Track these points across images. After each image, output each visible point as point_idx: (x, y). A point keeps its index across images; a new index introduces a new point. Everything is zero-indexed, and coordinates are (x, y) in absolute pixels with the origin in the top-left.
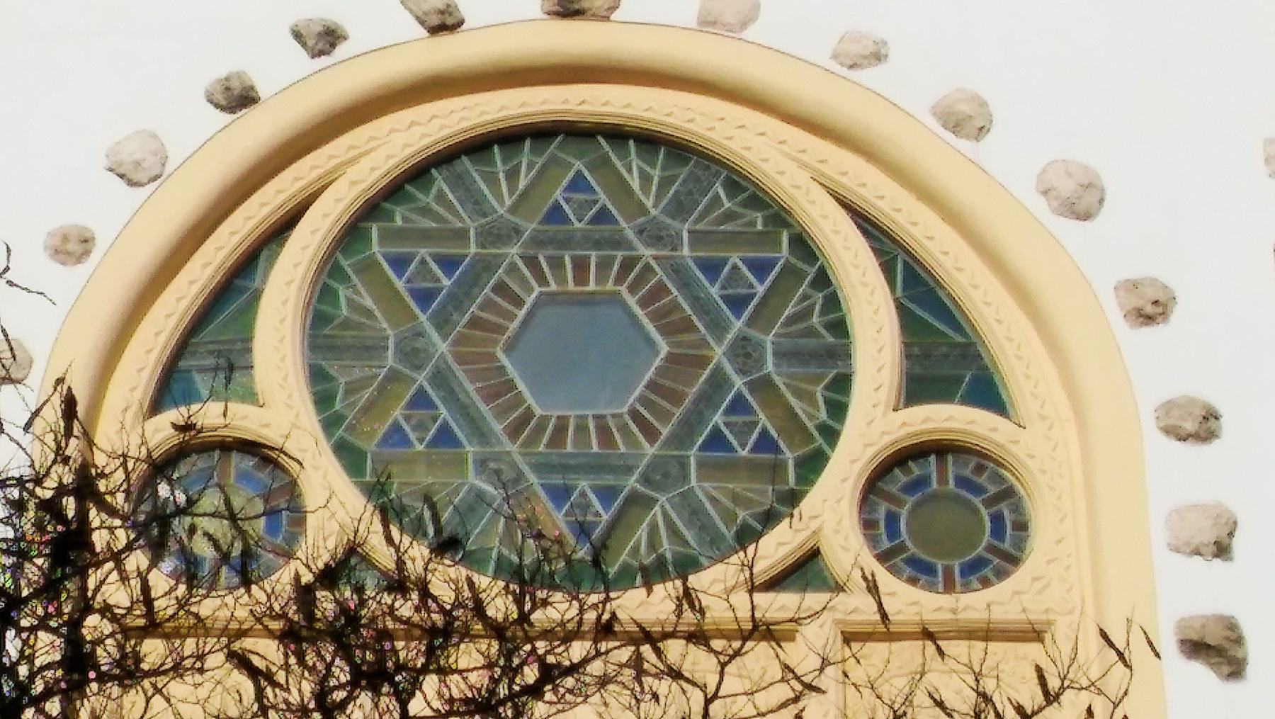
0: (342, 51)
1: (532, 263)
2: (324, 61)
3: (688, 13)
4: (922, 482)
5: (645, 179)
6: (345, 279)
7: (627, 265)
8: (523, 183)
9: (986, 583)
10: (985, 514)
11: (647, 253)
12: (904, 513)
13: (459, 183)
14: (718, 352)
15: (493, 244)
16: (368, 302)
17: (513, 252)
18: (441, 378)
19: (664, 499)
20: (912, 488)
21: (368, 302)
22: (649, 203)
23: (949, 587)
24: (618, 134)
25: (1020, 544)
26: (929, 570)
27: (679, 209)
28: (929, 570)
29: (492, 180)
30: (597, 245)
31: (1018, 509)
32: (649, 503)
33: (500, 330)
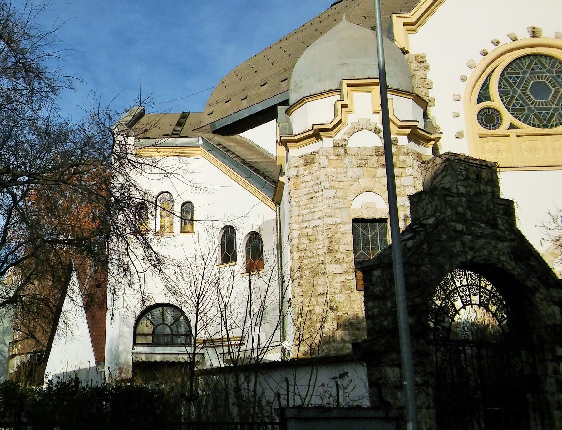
0: (500, 45)
1: (530, 77)
2: (497, 46)
3: (553, 36)
4: (486, 112)
5: (546, 63)
6: (502, 81)
7: (546, 76)
8: (527, 64)
9: (497, 129)
10: (496, 117)
11: (548, 75)
12: (483, 117)
13: (517, 64)
14: (519, 91)
15: (524, 74)
16: (506, 84)
17: (528, 75)
18: (520, 96)
19: (532, 114)
20: (484, 114)
21: (506, 84)
22: (547, 66)
23: (490, 129)
24: (541, 55)
25: (501, 122)
26: (487, 126)
27: (552, 67)
28: (487, 126)
29: (522, 63)
30: (540, 74)
31: (501, 116)
32: (554, 114)
33: (528, 88)
